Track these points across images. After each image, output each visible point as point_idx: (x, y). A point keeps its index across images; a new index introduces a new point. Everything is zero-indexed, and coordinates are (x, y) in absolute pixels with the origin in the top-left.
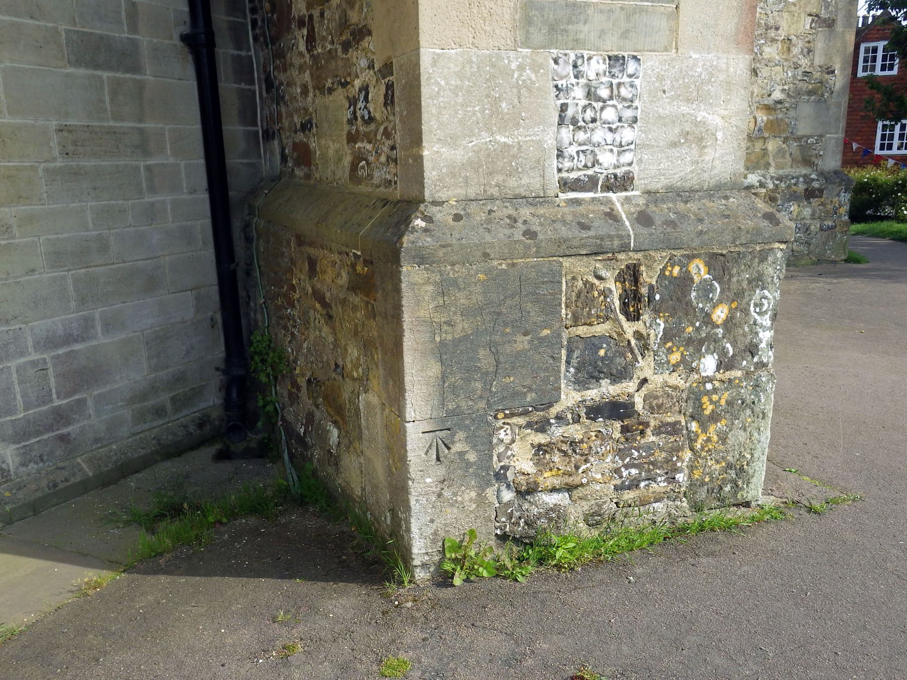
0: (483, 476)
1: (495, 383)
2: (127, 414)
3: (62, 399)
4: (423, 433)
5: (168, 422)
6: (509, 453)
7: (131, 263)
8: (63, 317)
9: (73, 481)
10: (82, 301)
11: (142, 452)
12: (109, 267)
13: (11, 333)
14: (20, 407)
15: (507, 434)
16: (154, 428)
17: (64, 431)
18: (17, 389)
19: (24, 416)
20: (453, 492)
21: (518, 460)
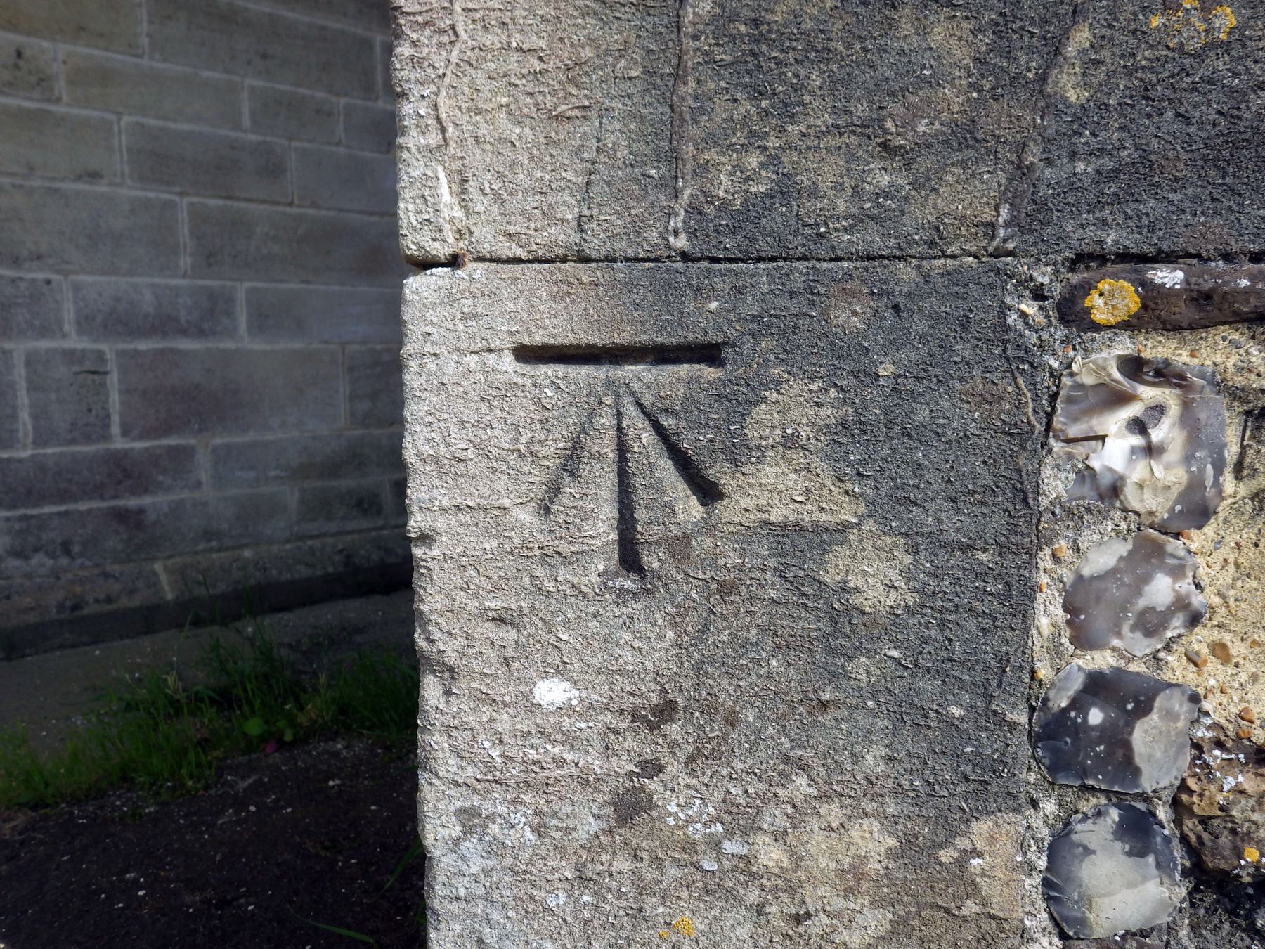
0: (953, 726)
1: (1081, 37)
2: (291, 496)
3: (134, 440)
4: (528, 354)
5: (383, 528)
6: (1161, 589)
7: (332, 213)
8: (157, 280)
9: (124, 602)
10: (209, 259)
11: (302, 572)
12: (281, 208)
13: (23, 285)
14: (26, 435)
15: (1151, 451)
16: (349, 533)
17: (132, 502)
18: (23, 398)
19: (32, 456)
20: (728, 804)
21: (1220, 651)
